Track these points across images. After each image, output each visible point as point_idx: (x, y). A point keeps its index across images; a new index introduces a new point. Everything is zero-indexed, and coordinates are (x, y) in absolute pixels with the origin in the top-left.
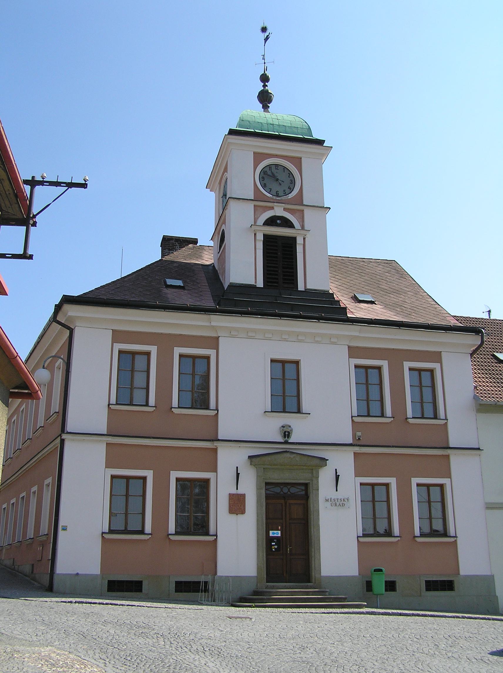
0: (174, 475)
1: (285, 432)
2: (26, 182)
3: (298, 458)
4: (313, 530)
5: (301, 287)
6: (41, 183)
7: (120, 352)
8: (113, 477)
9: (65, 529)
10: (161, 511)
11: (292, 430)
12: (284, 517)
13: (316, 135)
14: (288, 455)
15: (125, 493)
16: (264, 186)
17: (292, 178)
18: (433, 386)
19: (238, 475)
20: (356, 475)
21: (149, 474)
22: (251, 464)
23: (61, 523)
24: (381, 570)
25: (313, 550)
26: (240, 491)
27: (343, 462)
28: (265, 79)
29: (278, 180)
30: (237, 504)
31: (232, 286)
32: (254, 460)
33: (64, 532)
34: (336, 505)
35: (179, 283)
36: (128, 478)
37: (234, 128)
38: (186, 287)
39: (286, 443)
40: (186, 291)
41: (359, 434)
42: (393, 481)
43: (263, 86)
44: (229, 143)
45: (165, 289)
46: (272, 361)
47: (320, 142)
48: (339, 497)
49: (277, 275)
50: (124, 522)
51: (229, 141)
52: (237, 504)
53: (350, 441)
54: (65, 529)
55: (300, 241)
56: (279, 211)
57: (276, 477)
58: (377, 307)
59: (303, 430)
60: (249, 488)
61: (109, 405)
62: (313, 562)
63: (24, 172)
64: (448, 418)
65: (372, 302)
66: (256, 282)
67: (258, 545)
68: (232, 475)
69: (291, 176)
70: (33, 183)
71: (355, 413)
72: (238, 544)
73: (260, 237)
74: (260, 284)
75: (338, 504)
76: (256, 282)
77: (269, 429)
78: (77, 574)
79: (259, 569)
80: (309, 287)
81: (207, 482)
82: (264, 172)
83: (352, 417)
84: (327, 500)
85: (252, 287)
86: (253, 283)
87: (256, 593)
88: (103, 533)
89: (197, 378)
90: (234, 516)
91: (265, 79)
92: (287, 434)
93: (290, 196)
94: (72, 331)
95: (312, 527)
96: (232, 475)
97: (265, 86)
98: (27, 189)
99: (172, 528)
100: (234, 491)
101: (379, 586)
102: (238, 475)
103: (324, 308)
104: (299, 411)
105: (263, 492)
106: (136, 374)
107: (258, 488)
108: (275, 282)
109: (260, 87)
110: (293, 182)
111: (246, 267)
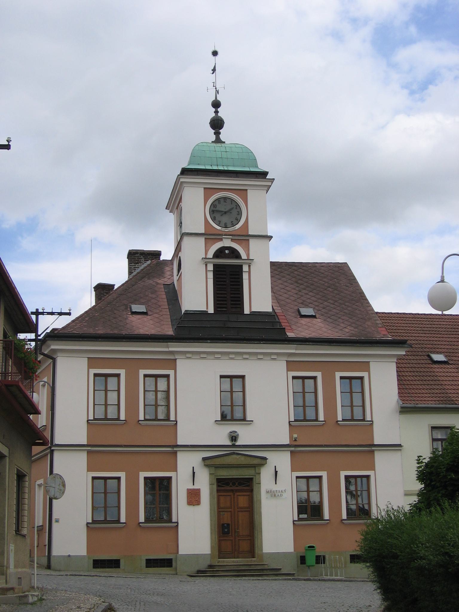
0: (143, 475)
1: (233, 437)
2: (33, 313)
3: (243, 458)
4: (256, 517)
5: (247, 311)
6: (42, 313)
7: (96, 375)
8: (94, 478)
9: (57, 521)
10: (132, 504)
11: (238, 435)
12: (233, 507)
13: (262, 167)
14: (235, 456)
15: (104, 494)
16: (214, 219)
17: (239, 210)
18: (363, 392)
19: (194, 473)
20: (293, 470)
21: (122, 475)
22: (409, 116)
23: (54, 516)
24: (313, 547)
25: (256, 532)
26: (196, 487)
27: (281, 461)
28: (216, 105)
29: (225, 211)
30: (194, 497)
31: (187, 313)
32: (206, 461)
33: (57, 523)
34: (275, 496)
35: (141, 308)
36: (105, 479)
37: (185, 165)
38: (149, 313)
39: (234, 446)
40: (149, 317)
41: (295, 436)
42: (324, 474)
43: (215, 112)
44: (182, 182)
45: (131, 316)
46: (222, 377)
47: (263, 175)
48: (278, 489)
49: (226, 301)
50: (104, 518)
51: (182, 180)
52: (194, 497)
53: (287, 442)
54: (57, 521)
55: (245, 268)
56: (227, 243)
57: (225, 474)
58: (318, 322)
59: (247, 436)
60: (204, 483)
61: (88, 421)
62: (256, 543)
63: (30, 307)
64: (374, 420)
65: (314, 317)
66: (207, 308)
67: (211, 529)
68: (189, 474)
69: (238, 207)
70: (37, 313)
71: (292, 419)
72: (195, 530)
73: (211, 267)
74: (211, 310)
75: (277, 495)
76: (207, 308)
77: (220, 436)
78: (69, 556)
79: (212, 548)
80: (253, 310)
81: (170, 479)
82: (213, 205)
83: (289, 422)
84: (267, 492)
85: (204, 313)
86: (206, 310)
87: (210, 566)
88: (88, 523)
89: (160, 395)
90: (191, 508)
91: (216, 105)
92: (234, 437)
93: (238, 226)
94: (54, 360)
95: (255, 514)
96: (189, 474)
97: (216, 112)
98: (34, 317)
99: (142, 519)
100: (191, 487)
101: (311, 560)
102: (194, 473)
103: (266, 331)
104: (244, 419)
105: (215, 487)
106: (109, 394)
107: (211, 484)
108: (232, 278)
109: (211, 113)
110: (240, 213)
111: (197, 294)
